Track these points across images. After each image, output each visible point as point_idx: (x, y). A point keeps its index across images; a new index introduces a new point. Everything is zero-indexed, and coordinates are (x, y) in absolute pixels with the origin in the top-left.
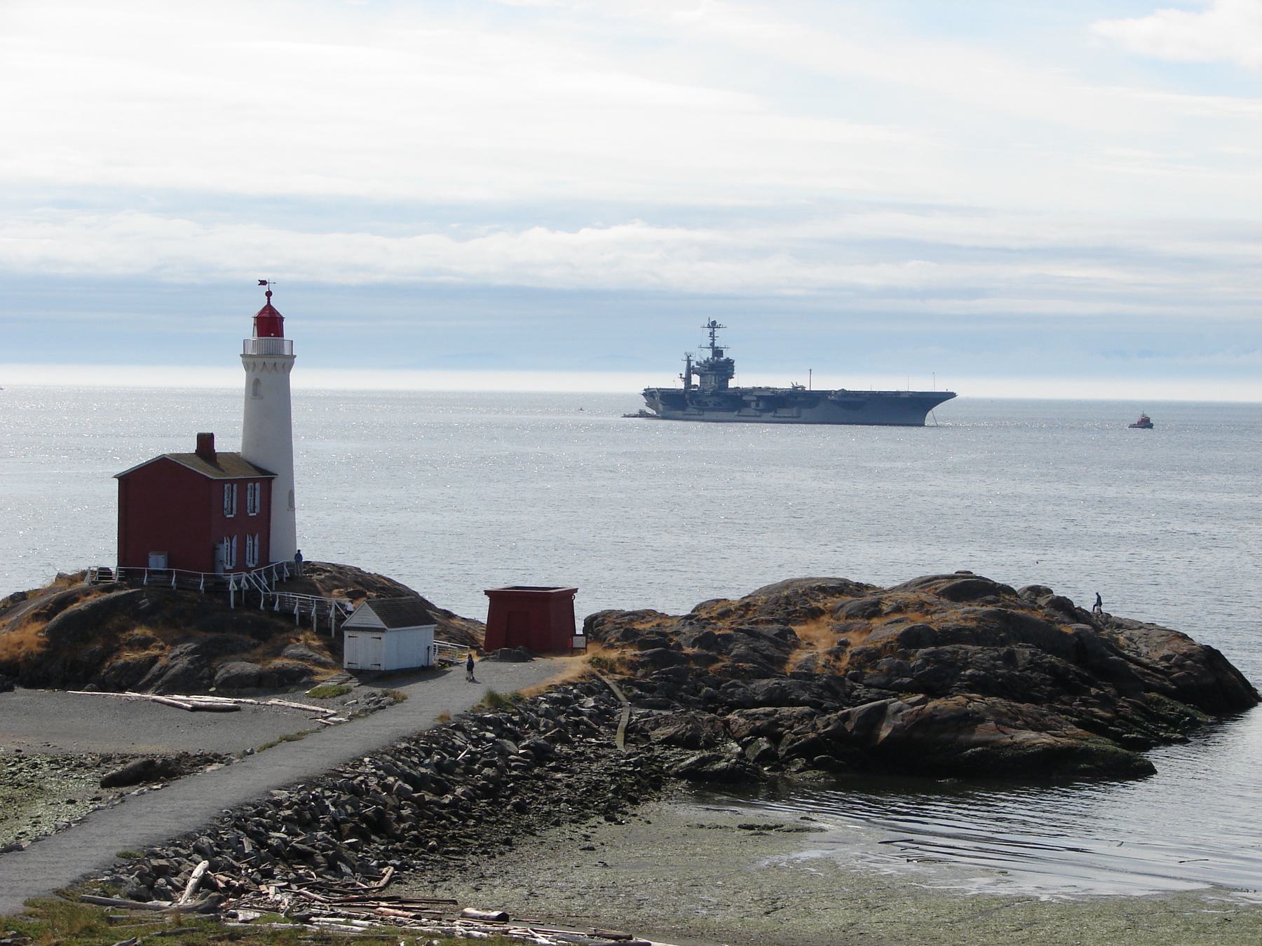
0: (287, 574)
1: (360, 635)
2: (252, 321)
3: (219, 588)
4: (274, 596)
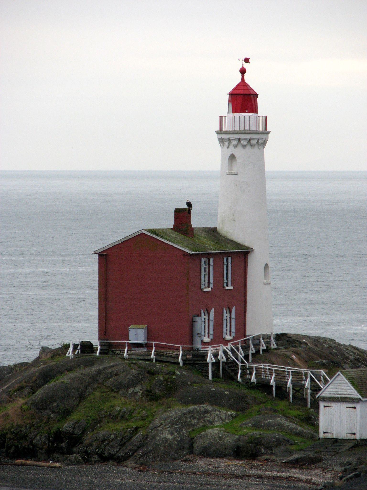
0: (263, 346)
1: (336, 406)
2: (227, 98)
3: (196, 361)
4: (251, 368)
